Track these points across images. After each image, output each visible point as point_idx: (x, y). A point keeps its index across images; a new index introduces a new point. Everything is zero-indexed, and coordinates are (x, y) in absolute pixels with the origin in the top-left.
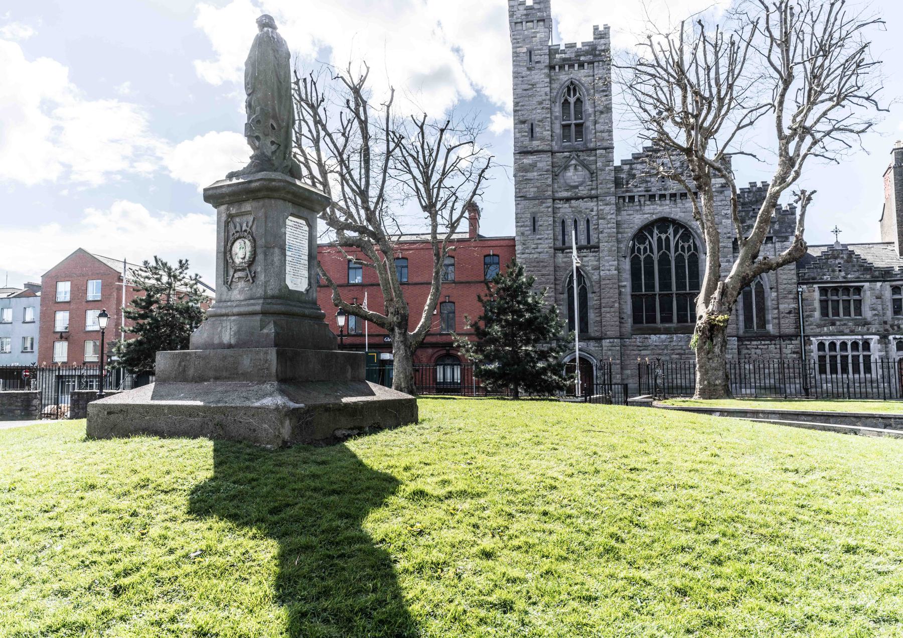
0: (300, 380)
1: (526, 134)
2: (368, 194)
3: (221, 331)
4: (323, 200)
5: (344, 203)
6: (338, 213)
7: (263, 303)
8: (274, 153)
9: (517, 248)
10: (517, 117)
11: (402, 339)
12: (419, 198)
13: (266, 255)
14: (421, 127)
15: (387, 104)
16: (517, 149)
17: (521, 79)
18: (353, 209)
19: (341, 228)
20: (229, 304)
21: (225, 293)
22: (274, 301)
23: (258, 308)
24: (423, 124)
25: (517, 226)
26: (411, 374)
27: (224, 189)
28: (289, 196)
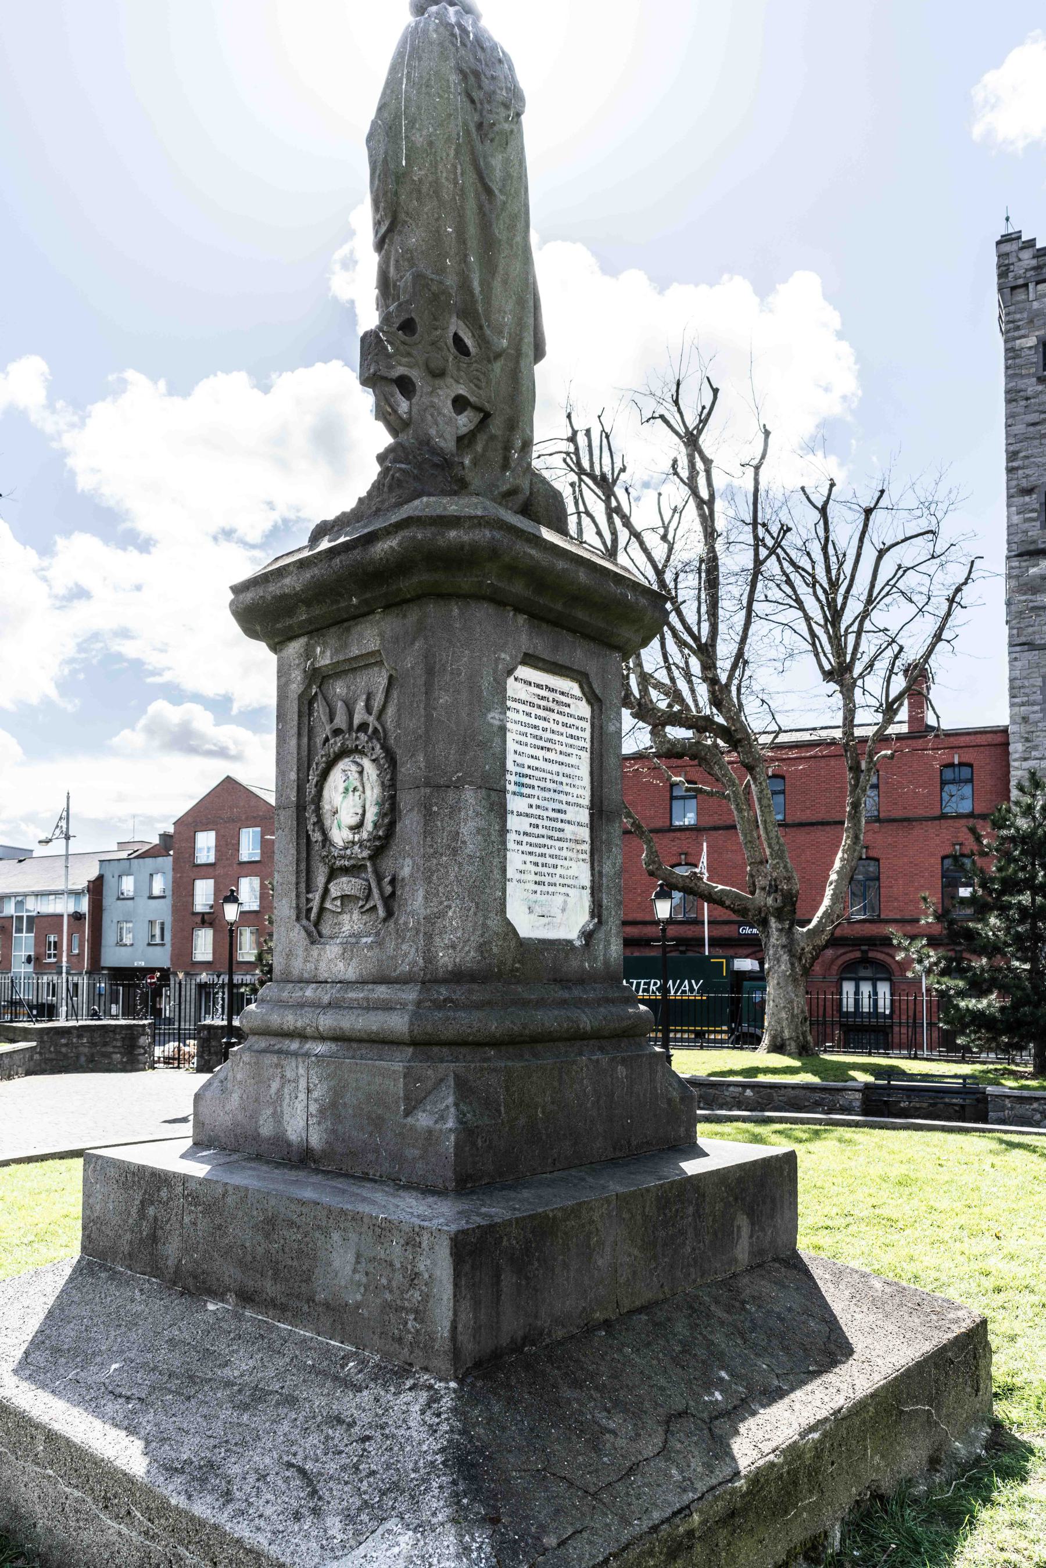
0: (560, 1333)
1: (1034, 515)
2: (714, 651)
3: (279, 1093)
4: (643, 601)
5: (664, 672)
6: (654, 694)
7: (419, 1003)
8: (464, 441)
9: (1011, 748)
10: (1014, 483)
11: (784, 940)
12: (817, 655)
13: (429, 816)
14: (823, 511)
15: (755, 463)
16: (1014, 547)
17: (1023, 403)
18: (682, 685)
19: (657, 721)
20: (309, 992)
21: (300, 952)
22: (459, 993)
23: (398, 1023)
24: (826, 503)
25: (1012, 705)
26: (803, 1012)
27: (287, 581)
28: (518, 588)
